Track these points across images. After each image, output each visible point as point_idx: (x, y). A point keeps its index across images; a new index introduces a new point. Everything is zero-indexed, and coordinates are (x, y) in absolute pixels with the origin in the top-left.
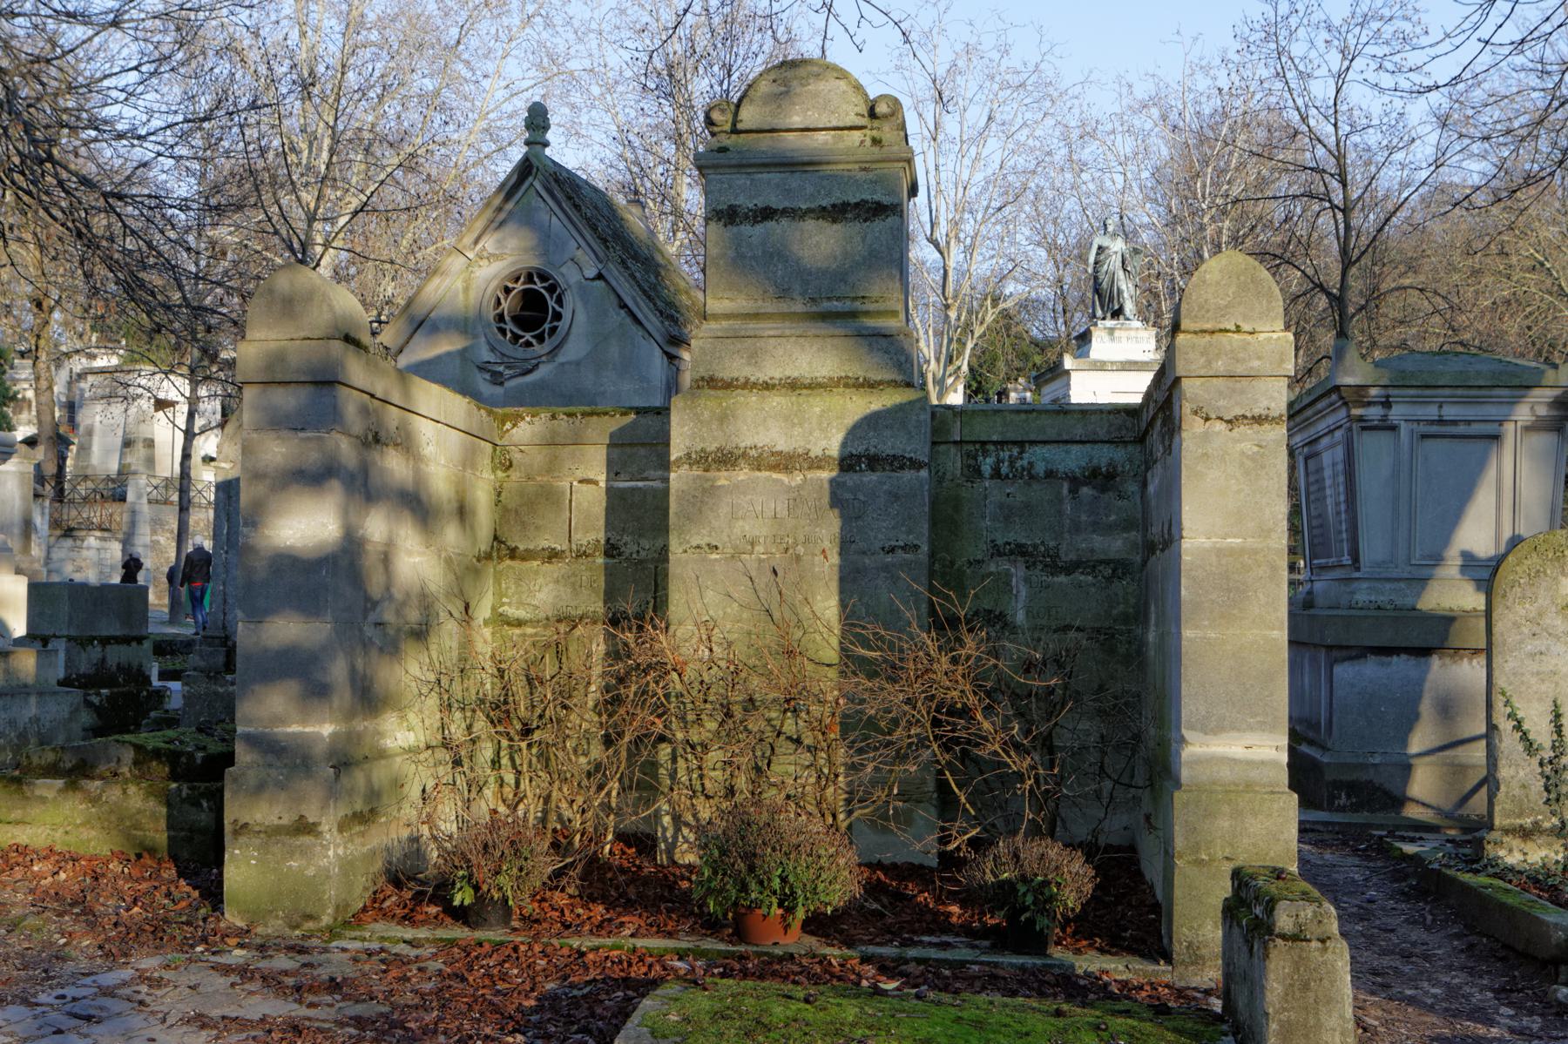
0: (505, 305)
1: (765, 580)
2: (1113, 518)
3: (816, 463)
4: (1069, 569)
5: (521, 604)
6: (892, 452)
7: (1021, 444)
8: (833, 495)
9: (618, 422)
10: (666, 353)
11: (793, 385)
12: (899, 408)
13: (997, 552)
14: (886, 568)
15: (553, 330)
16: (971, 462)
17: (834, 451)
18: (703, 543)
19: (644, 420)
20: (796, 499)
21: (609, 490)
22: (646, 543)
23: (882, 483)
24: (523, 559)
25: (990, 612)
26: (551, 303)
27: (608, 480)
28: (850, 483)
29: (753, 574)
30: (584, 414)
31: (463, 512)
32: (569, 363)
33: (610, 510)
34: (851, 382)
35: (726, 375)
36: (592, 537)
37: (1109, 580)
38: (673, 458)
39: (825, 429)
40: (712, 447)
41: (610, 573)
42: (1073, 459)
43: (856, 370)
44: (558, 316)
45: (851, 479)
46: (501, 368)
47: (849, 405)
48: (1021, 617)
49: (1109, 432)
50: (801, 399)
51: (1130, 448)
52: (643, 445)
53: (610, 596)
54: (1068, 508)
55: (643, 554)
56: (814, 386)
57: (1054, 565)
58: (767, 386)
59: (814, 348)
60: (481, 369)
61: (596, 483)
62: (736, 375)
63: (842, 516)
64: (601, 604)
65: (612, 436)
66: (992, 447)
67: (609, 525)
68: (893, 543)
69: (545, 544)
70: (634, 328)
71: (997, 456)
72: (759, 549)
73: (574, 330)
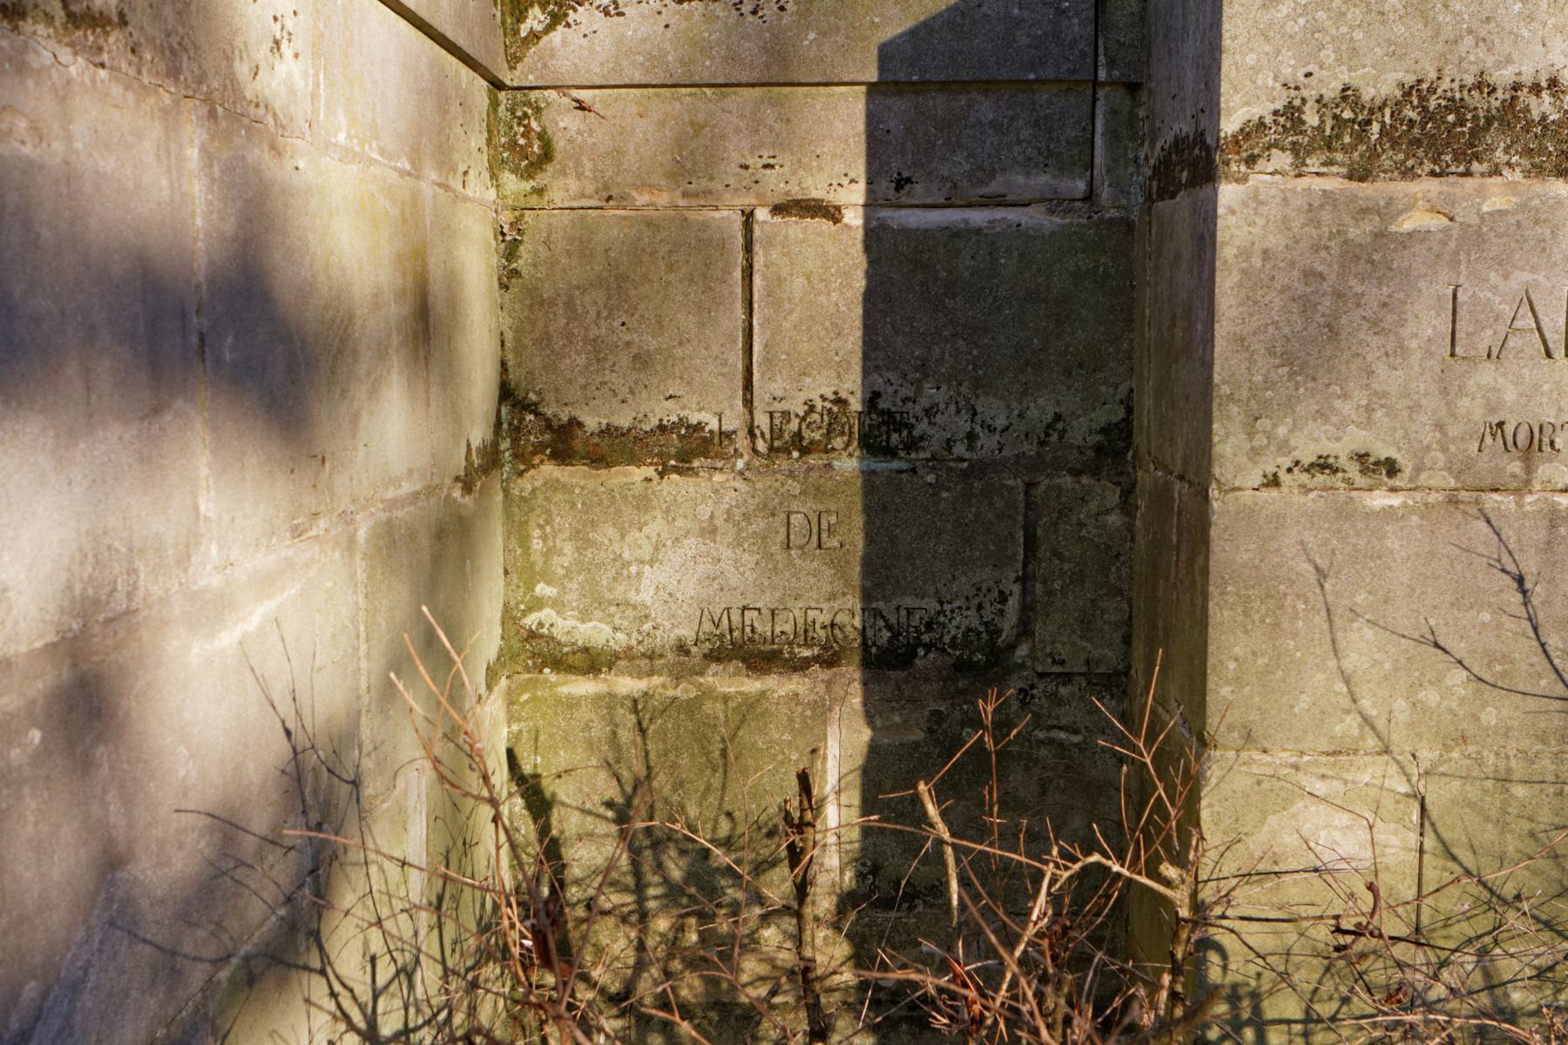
5: (595, 603)
18: (1340, 451)
21: (874, 236)
24: (598, 460)
31: (425, 325)
33: (879, 302)
36: (820, 387)
38: (1229, 126)
40: (1379, 84)
41: (879, 501)
52: (988, 85)
53: (879, 575)
55: (988, 443)
61: (832, 213)
64: (854, 602)
65: (886, 54)
67: (876, 350)
69: (668, 412)
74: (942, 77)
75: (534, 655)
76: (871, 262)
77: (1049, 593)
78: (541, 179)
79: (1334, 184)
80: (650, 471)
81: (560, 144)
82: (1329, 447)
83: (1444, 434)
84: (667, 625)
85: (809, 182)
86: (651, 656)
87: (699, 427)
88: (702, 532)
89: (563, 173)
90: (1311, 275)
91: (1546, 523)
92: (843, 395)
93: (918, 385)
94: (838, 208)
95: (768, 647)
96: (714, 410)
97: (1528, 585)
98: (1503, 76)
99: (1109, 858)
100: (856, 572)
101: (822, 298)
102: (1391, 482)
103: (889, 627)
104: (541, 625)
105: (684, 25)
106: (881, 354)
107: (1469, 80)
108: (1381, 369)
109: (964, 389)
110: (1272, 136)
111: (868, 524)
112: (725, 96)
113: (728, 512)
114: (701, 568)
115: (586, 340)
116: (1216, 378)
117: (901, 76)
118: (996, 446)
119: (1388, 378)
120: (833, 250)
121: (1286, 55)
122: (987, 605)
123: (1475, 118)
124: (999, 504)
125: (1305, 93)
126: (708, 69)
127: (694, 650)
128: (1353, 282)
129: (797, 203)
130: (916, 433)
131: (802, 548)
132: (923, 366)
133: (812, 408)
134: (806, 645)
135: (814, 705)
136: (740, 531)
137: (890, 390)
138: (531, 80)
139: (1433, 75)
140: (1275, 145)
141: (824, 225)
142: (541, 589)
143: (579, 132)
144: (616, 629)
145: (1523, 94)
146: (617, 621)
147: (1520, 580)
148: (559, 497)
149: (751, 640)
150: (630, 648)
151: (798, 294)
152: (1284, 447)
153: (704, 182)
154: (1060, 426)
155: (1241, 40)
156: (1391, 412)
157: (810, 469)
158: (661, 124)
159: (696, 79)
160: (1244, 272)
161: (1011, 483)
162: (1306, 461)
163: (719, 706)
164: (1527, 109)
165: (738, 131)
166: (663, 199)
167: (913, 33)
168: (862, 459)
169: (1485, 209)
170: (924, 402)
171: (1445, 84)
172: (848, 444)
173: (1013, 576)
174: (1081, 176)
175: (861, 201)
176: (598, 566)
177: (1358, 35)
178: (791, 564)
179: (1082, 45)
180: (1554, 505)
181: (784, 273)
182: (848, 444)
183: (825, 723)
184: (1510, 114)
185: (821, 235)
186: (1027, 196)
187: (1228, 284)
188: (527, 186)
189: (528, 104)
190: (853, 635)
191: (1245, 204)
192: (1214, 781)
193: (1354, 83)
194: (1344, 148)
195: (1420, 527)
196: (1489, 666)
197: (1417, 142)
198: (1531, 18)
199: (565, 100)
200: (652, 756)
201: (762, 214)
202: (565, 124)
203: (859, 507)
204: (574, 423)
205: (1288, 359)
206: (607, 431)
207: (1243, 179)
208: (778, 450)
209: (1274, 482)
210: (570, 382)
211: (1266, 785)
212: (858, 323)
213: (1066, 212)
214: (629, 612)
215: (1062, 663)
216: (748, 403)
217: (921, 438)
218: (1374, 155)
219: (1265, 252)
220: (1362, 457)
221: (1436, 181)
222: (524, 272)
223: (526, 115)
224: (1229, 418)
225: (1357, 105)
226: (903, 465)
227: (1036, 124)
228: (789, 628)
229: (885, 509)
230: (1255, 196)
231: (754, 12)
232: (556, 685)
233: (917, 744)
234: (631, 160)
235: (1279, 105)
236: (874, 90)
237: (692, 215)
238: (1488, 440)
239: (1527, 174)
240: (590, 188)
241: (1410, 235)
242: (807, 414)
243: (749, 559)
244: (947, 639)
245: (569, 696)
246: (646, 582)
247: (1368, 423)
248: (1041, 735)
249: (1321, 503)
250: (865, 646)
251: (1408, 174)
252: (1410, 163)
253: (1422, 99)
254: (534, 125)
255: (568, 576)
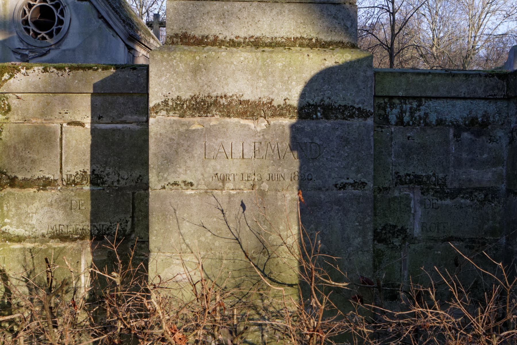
0: (29, 15)
1: (234, 212)
2: (485, 156)
3: (280, 111)
4: (453, 194)
6: (343, 103)
7: (418, 99)
8: (293, 138)
9: (99, 76)
10: (127, 45)
11: (256, 44)
12: (349, 65)
13: (400, 181)
14: (338, 202)
15: (58, 30)
16: (382, 112)
17: (294, 101)
18: (179, 180)
19: (121, 74)
20: (261, 146)
21: (93, 131)
22: (124, 174)
23: (335, 129)
24: (22, 187)
25: (395, 227)
26: (57, 14)
27: (92, 123)
28: (308, 129)
29: (225, 207)
30: (71, 68)
32: (69, 50)
33: (94, 147)
34: (305, 42)
35: (198, 33)
36: (79, 168)
37: (482, 202)
38: (151, 105)
39: (289, 78)
40: (186, 95)
41: (94, 197)
42: (457, 111)
43: (310, 32)
44: (61, 22)
45: (308, 125)
46: (27, 52)
47: (307, 61)
48: (417, 231)
49: (485, 91)
50: (265, 55)
51: (499, 103)
52: (121, 94)
53: (95, 216)
54: (453, 148)
55: (122, 182)
56: (274, 44)
57: (442, 193)
58: (234, 44)
59: (274, 12)
60: (15, 52)
61: (82, 125)
62: (206, 33)
63: (300, 157)
64: (88, 223)
65: (95, 86)
66: (397, 101)
68: (345, 181)
70: (107, 30)
71: (401, 107)
72: (230, 185)
73: (71, 31)
74: (109, 92)
75: (4, 238)
76: (92, 137)
77: (138, 220)
78: (8, 116)
79: (176, 118)
80: (35, 190)
81: (13, 107)
82: (177, 180)
83: (204, 176)
84: (40, 229)
85: (76, 117)
86: (35, 238)
87: (48, 178)
88: (49, 205)
89: (14, 114)
90: (171, 139)
91: (228, 197)
92: (85, 170)
93: (105, 168)
94: (84, 124)
95: (66, 235)
96: (53, 175)
97: (224, 212)
98: (214, 94)
99: (96, 269)
100: (89, 215)
101: (80, 146)
102: (192, 188)
103: (98, 230)
104: (6, 230)
105: (44, 78)
106: (95, 160)
107: (206, 95)
108: (188, 161)
109: (117, 169)
110: (161, 107)
111: (92, 203)
112: (55, 96)
113: (56, 200)
114: (48, 215)
115: (19, 156)
116: (150, 163)
117: (99, 91)
118: (124, 183)
119: (190, 163)
120: (83, 134)
121: (164, 89)
122: (123, 224)
123: (208, 104)
124: (126, 198)
125: (169, 97)
126: (50, 89)
127: (46, 236)
128: (181, 141)
129: (73, 122)
130: (104, 180)
131: (75, 209)
132: (106, 163)
133: (77, 174)
134: (76, 234)
135: (78, 250)
136: (59, 205)
137: (98, 169)
138: (5, 91)
139: (198, 94)
140: (162, 109)
141: (80, 128)
142: (6, 220)
143: (18, 104)
144: (26, 231)
145: (219, 98)
146: (26, 228)
147: (222, 211)
148: (11, 196)
149: (62, 233)
150: (30, 236)
151: (74, 145)
152: (166, 179)
153: (50, 117)
154: (141, 178)
155: (154, 85)
156: (191, 171)
157: (77, 189)
158: (39, 102)
159: (47, 91)
160: (156, 138)
161: (128, 192)
162: (171, 183)
163: (53, 251)
164: (220, 102)
165: (58, 104)
166: (39, 121)
167: (102, 81)
168: (90, 186)
169: (211, 124)
170: (106, 172)
171: (201, 96)
172: (87, 183)
173: (129, 216)
174: (145, 116)
175: (90, 122)
176: (21, 214)
177: (181, 85)
178: (72, 213)
179: (144, 85)
180: (230, 193)
181: (70, 139)
182: (87, 183)
183: (81, 255)
184: (216, 103)
185: (80, 130)
186: (131, 121)
187: (152, 141)
188: (4, 117)
189: (5, 97)
190: (88, 232)
191: (155, 123)
192: (151, 260)
193: (180, 95)
194: (178, 110)
195: (199, 198)
196: (216, 231)
197: (195, 109)
198: (220, 81)
199: (14, 96)
200: (35, 264)
201: (65, 125)
202: (14, 102)
203: (90, 199)
204: (16, 177)
205: (166, 159)
206: (24, 179)
207: (155, 117)
208: (69, 184)
209: (164, 188)
210: (15, 167)
211: (164, 261)
212: (89, 152)
213: (141, 125)
214: (29, 226)
215: (142, 238)
216: (61, 172)
217: (106, 181)
218: (185, 112)
219: (161, 134)
220: (184, 182)
221: (199, 118)
222: (3, 139)
223: (4, 100)
224: (153, 173)
225: (180, 100)
226: (101, 188)
227: (134, 104)
228: (71, 230)
229: (96, 199)
230: (158, 121)
231: (62, 75)
232: (10, 245)
233: (105, 260)
234: (31, 111)
235: (163, 100)
236: (93, 95)
237: (46, 125)
238: (214, 178)
239: (220, 116)
240: (20, 118)
241: (194, 130)
242: (76, 175)
243: (61, 212)
244: (112, 232)
245: (13, 248)
246: (34, 218)
247: (186, 174)
248: (137, 257)
249: (175, 193)
250: (91, 235)
251: (193, 116)
252: (193, 114)
253: (196, 99)
254: (6, 102)
255: (13, 217)
